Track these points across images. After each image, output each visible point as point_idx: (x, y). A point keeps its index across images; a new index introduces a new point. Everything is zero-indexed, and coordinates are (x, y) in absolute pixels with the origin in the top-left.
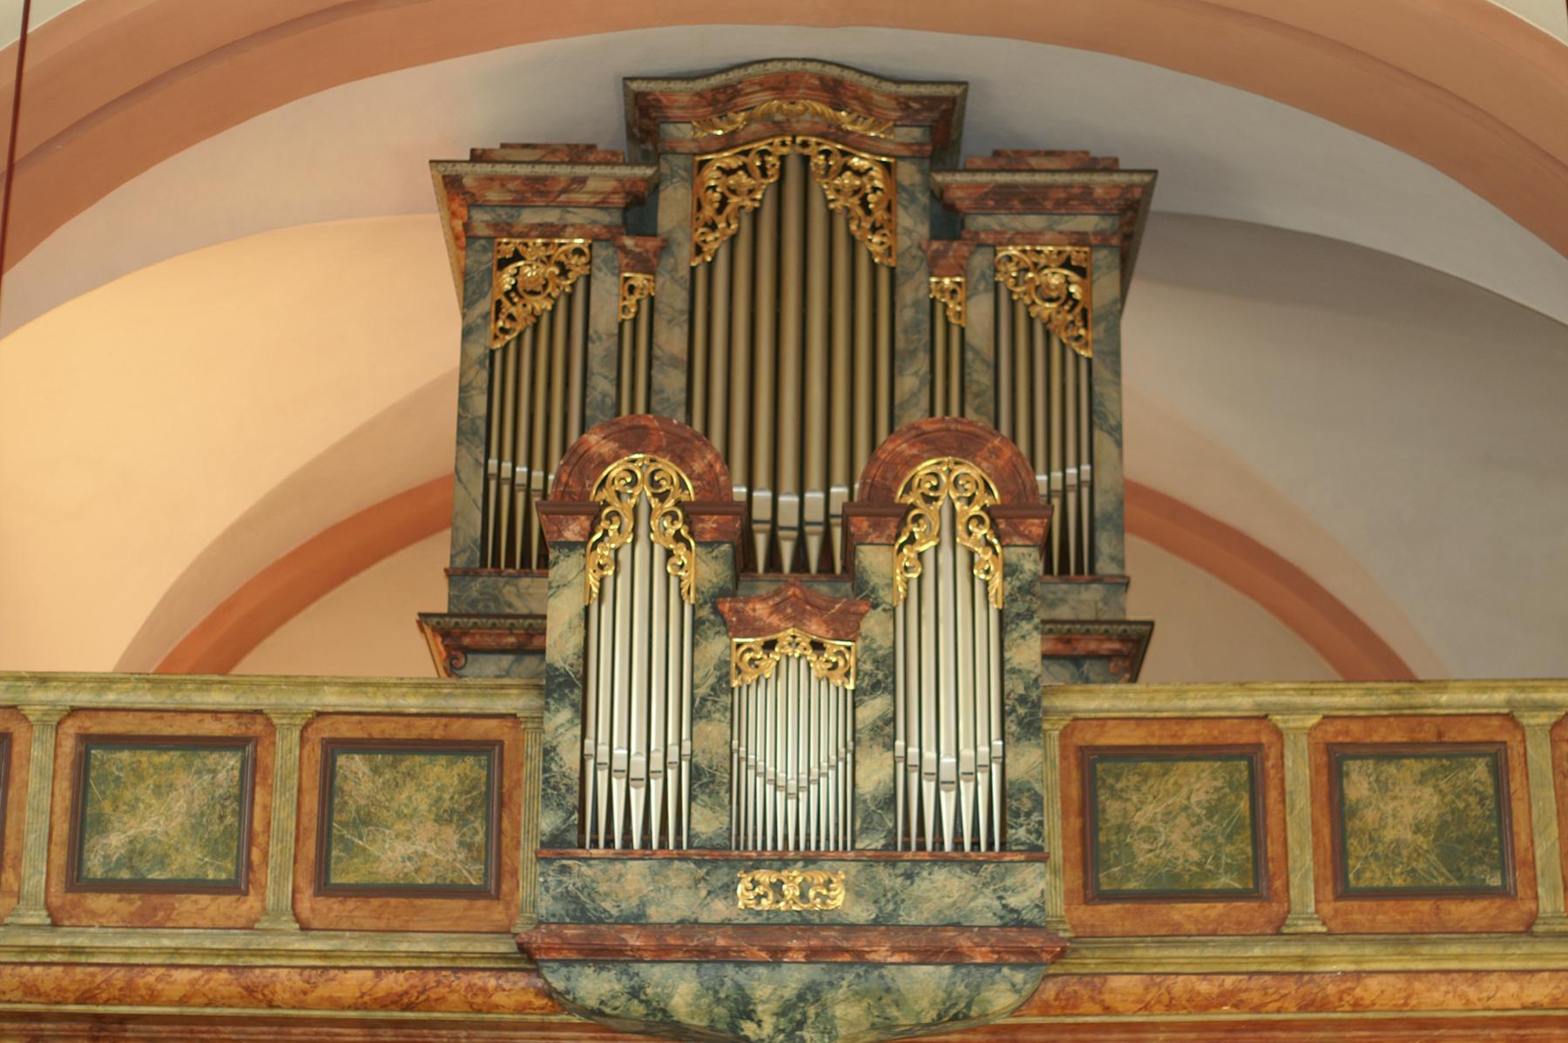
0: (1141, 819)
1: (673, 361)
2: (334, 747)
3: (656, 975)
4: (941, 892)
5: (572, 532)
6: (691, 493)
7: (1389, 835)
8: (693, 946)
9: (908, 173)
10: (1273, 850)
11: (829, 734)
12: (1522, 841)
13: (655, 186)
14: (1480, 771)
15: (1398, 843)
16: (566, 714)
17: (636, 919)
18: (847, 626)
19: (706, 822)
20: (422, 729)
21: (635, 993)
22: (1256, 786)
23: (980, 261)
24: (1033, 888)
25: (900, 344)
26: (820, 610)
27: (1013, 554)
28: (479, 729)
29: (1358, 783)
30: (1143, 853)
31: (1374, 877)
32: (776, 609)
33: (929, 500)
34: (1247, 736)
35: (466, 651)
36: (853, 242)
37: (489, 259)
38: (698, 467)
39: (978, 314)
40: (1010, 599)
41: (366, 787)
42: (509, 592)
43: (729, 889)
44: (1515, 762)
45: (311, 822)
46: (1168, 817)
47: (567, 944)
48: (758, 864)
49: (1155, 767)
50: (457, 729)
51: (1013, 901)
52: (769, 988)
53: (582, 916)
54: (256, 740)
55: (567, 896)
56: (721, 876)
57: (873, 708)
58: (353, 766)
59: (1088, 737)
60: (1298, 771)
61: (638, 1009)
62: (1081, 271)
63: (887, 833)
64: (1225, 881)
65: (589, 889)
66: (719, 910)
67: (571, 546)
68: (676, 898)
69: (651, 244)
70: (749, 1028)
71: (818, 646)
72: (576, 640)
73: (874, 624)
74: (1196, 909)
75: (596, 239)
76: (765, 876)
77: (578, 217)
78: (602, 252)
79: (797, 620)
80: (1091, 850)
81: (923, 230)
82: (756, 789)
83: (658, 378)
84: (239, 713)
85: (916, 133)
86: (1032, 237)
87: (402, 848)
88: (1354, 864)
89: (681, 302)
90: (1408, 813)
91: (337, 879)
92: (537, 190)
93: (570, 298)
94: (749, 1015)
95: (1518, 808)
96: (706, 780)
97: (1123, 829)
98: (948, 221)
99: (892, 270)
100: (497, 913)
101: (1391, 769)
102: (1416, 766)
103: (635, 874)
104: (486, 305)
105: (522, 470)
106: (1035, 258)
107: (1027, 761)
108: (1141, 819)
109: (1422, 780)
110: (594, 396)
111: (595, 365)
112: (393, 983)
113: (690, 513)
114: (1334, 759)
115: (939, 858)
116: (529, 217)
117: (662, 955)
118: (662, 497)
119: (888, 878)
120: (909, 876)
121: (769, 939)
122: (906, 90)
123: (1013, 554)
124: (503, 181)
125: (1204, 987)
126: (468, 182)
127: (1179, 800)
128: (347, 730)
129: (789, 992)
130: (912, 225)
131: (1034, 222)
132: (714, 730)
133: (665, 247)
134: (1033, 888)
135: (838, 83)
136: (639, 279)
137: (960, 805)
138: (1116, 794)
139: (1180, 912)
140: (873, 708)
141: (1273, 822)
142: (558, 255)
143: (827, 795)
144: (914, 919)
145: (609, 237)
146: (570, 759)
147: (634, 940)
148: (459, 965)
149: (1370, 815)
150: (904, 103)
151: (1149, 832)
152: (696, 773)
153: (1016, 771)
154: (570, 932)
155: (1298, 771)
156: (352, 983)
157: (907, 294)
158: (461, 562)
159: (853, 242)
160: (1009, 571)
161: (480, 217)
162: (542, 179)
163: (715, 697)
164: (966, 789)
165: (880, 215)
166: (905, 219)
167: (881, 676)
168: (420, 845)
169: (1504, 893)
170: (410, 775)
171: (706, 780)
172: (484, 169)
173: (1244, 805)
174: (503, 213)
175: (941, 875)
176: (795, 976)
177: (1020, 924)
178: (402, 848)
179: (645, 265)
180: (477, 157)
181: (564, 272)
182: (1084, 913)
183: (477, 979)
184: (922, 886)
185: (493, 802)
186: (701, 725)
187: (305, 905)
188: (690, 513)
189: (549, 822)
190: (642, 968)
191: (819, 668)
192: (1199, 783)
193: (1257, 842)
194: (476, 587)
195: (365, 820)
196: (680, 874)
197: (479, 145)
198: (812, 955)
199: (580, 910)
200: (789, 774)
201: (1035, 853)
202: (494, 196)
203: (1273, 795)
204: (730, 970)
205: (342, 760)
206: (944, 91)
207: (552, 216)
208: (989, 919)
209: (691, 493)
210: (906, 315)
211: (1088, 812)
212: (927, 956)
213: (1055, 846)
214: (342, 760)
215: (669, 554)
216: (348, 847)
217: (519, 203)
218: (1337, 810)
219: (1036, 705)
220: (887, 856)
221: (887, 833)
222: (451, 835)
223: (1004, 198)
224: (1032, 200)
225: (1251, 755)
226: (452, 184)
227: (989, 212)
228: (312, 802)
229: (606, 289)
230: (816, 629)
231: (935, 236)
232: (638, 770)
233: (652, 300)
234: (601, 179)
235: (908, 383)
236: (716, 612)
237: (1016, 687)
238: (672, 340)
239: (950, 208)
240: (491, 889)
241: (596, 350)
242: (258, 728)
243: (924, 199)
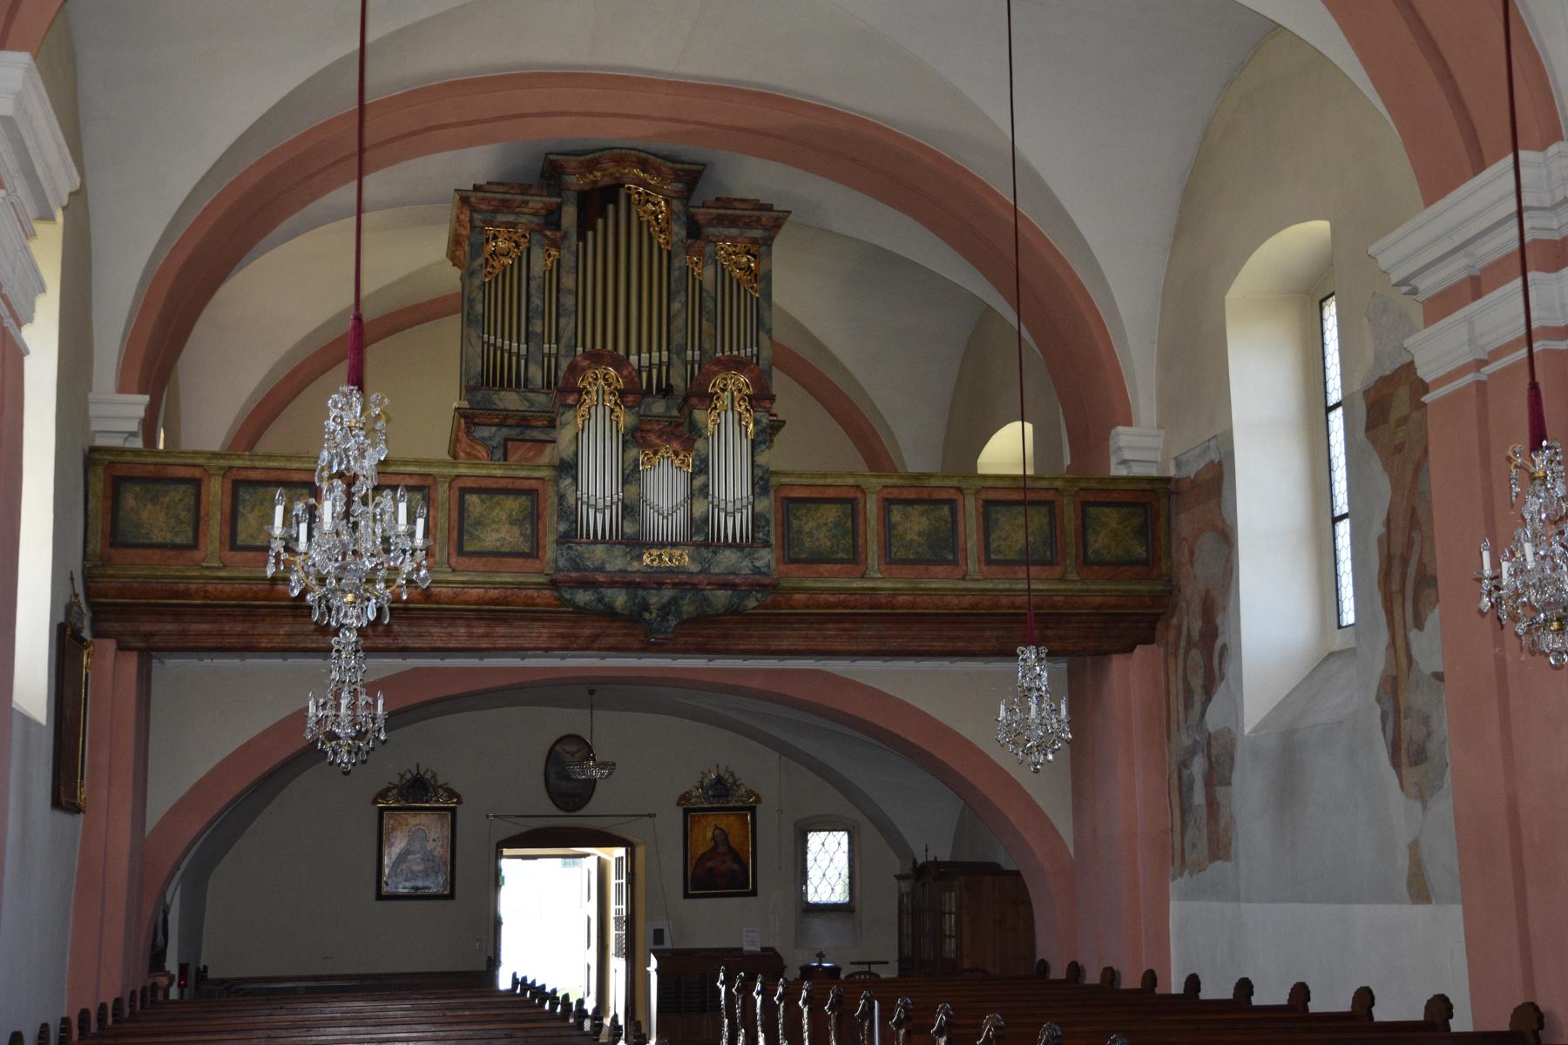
0: (807, 528)
1: (569, 292)
2: (464, 491)
3: (609, 593)
4: (728, 558)
5: (570, 400)
6: (621, 385)
7: (908, 537)
8: (628, 583)
9: (676, 205)
10: (861, 542)
11: (680, 494)
12: (961, 541)
13: (559, 207)
14: (946, 510)
15: (911, 541)
16: (569, 481)
17: (601, 569)
18: (688, 445)
19: (629, 529)
20: (503, 483)
21: (600, 600)
22: (854, 515)
23: (709, 249)
24: (765, 557)
25: (673, 287)
26: (678, 437)
27: (758, 415)
28: (528, 484)
29: (896, 515)
30: (808, 543)
31: (901, 554)
32: (659, 437)
33: (723, 390)
34: (851, 494)
35: (476, 424)
36: (650, 236)
37: (483, 238)
38: (625, 372)
39: (708, 274)
40: (757, 434)
41: (479, 509)
42: (495, 397)
43: (639, 558)
44: (960, 507)
45: (455, 524)
46: (818, 527)
47: (572, 580)
48: (652, 545)
49: (813, 506)
50: (518, 485)
51: (757, 564)
52: (655, 599)
53: (577, 568)
54: (429, 487)
55: (571, 559)
56: (636, 552)
57: (699, 481)
58: (472, 499)
59: (785, 493)
60: (872, 508)
61: (601, 607)
62: (754, 256)
63: (701, 534)
64: (841, 555)
65: (580, 556)
66: (635, 566)
67: (571, 407)
68: (617, 562)
69: (559, 234)
70: (646, 615)
71: (677, 454)
72: (573, 448)
73: (699, 444)
74: (829, 566)
75: (532, 230)
76: (655, 552)
77: (523, 219)
78: (536, 237)
79: (668, 441)
80: (788, 541)
81: (683, 233)
82: (650, 515)
83: (563, 300)
84: (420, 475)
85: (680, 186)
86: (733, 239)
87: (495, 536)
88: (894, 549)
89: (573, 264)
90: (916, 528)
91: (468, 548)
92: (505, 206)
93: (520, 258)
94: (648, 610)
95: (961, 528)
96: (630, 510)
97: (800, 532)
98: (694, 230)
99: (669, 252)
100: (537, 565)
101: (910, 509)
102: (919, 508)
103: (600, 550)
104: (481, 260)
105: (507, 342)
106: (727, 247)
107: (764, 505)
108: (807, 528)
109: (922, 514)
110: (532, 306)
111: (533, 291)
112: (494, 593)
113: (622, 394)
114: (888, 503)
115: (727, 545)
116: (500, 218)
117: (612, 584)
118: (609, 385)
119: (706, 553)
120: (715, 553)
121: (656, 580)
122: (678, 166)
123: (758, 415)
124: (489, 201)
125: (832, 599)
126: (473, 200)
127: (822, 521)
128: (469, 483)
129: (665, 600)
130: (679, 231)
131: (734, 231)
132: (632, 489)
133: (565, 236)
134: (765, 557)
135: (646, 160)
136: (553, 252)
137: (733, 524)
138: (798, 518)
139: (823, 568)
140: (699, 481)
141: (861, 531)
142: (515, 237)
143: (679, 518)
144: (716, 570)
145: (539, 230)
146: (571, 500)
147: (600, 578)
148: (521, 586)
149: (901, 529)
150: (676, 172)
151: (810, 534)
152: (625, 507)
153: (760, 507)
154: (573, 575)
155: (872, 508)
156: (475, 592)
157: (676, 263)
158: (472, 383)
159: (650, 236)
160: (756, 423)
161: (477, 216)
162: (507, 201)
163: (631, 476)
164: (738, 516)
165: (664, 225)
166: (675, 228)
167: (702, 468)
168: (503, 534)
169: (955, 563)
170: (497, 503)
171: (630, 510)
172: (480, 194)
173: (849, 524)
174: (488, 216)
175: (727, 553)
176: (667, 594)
177: (760, 573)
178: (495, 536)
179: (556, 245)
180: (476, 188)
181: (517, 245)
182: (784, 568)
183: (529, 592)
184: (719, 557)
185: (534, 517)
186: (627, 487)
187: (453, 560)
188: (622, 394)
189: (563, 527)
190: (603, 590)
191: (677, 462)
192: (831, 513)
193: (854, 538)
194: (479, 395)
195: (478, 523)
196: (618, 550)
197: (479, 182)
198: (674, 585)
199: (576, 564)
200: (665, 505)
201: (766, 544)
202: (484, 207)
203: (861, 520)
204: (640, 592)
205: (467, 497)
206: (694, 167)
207: (511, 218)
208: (747, 571)
209: (621, 385)
210: (675, 274)
211: (786, 525)
212: (722, 586)
213: (773, 540)
214: (467, 497)
215: (612, 411)
216: (471, 535)
217: (496, 211)
218: (887, 527)
219: (767, 481)
220: (705, 545)
221: (701, 534)
222: (516, 530)
223: (721, 221)
224: (733, 222)
225: (852, 501)
226: (464, 199)
227: (713, 226)
228: (455, 515)
229: (537, 255)
230: (676, 445)
231: (689, 236)
232: (600, 505)
233: (559, 261)
234: (537, 203)
235: (676, 306)
236: (635, 438)
237: (759, 473)
238: (568, 281)
239: (696, 223)
240: (534, 553)
241: (533, 284)
242: (429, 482)
243: (684, 218)
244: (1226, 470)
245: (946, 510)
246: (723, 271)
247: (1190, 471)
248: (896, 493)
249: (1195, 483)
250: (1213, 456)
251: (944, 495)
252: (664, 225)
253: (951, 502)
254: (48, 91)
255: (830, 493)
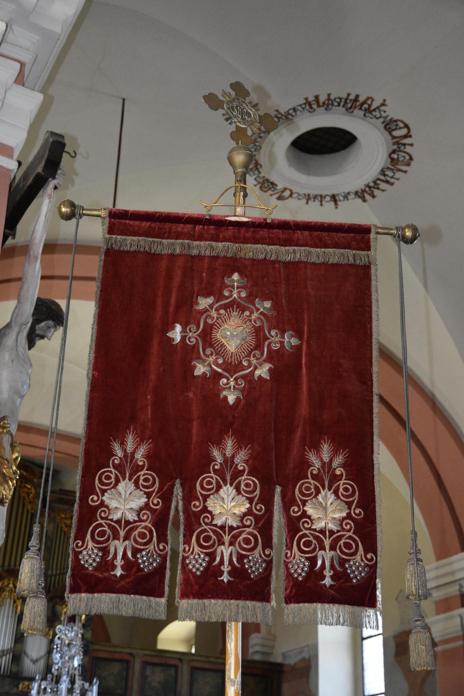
10: (129, 685)
14: (172, 671)
19: (14, 669)
22: (127, 669)
36: (24, 505)
43: (17, 686)
60: (137, 666)
66: (15, 690)
95: (179, 681)
114: (145, 664)
132: (19, 646)
155: (137, 666)
173: (125, 674)
218: (143, 677)
244: (313, 664)
245: (172, 671)
246: (58, 526)
247: (292, 661)
248: (149, 659)
249: (293, 668)
250: (305, 655)
251: (173, 662)
252: (32, 500)
253: (176, 667)
254: (370, 295)
255: (117, 656)
